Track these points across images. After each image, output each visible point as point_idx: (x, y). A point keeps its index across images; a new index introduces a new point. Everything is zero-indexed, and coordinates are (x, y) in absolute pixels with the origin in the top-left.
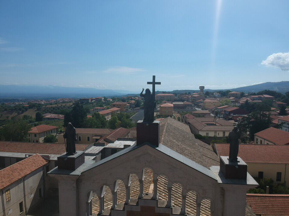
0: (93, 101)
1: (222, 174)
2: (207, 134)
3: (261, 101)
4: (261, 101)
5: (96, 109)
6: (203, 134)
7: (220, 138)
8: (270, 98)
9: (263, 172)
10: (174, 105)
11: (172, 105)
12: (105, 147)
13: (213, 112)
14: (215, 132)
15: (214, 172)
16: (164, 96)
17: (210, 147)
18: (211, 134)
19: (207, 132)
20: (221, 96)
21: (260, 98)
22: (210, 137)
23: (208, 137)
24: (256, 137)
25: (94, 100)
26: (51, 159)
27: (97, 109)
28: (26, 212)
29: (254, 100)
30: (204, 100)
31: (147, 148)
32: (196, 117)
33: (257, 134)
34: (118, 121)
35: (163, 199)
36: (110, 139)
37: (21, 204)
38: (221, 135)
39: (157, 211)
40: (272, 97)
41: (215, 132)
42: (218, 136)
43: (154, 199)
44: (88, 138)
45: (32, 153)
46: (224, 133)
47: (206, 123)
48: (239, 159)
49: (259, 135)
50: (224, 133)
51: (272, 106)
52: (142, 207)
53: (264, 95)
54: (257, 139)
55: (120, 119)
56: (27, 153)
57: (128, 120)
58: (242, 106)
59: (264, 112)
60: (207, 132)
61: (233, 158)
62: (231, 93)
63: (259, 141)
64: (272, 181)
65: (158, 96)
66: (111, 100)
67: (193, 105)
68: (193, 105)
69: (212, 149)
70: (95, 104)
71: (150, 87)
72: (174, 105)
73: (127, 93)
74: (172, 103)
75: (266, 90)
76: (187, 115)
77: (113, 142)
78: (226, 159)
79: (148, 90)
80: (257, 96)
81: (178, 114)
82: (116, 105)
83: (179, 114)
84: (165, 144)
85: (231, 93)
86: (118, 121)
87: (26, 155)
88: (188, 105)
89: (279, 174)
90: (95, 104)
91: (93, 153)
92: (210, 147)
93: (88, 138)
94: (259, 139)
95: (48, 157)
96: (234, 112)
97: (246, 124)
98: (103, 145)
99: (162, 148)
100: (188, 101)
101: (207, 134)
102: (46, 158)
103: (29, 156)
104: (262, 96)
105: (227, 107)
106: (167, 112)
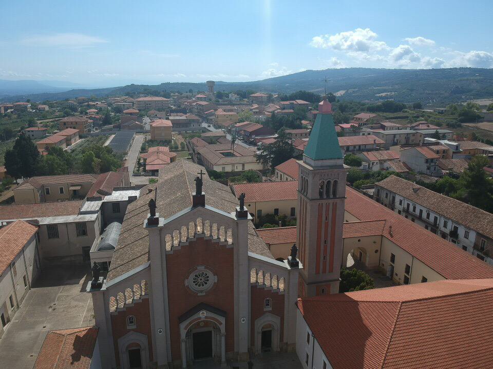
0: (9, 111)
1: (237, 216)
2: (224, 168)
3: (292, 111)
4: (292, 111)
5: (29, 131)
6: (218, 169)
7: (238, 173)
8: (306, 104)
9: (278, 209)
10: (173, 122)
11: (168, 123)
12: (103, 201)
13: (229, 132)
14: (233, 165)
15: (233, 215)
16: (150, 101)
17: (228, 188)
18: (229, 169)
19: (223, 166)
20: (240, 100)
21: (292, 106)
22: (227, 172)
23: (225, 173)
24: (277, 171)
25: (11, 108)
26: (40, 224)
27: (32, 131)
28: (29, 286)
29: (284, 109)
30: (216, 110)
31: (200, 208)
32: (209, 143)
33: (276, 167)
34: (95, 159)
35: (207, 233)
36: (104, 189)
37: (24, 277)
38: (240, 169)
39: (205, 239)
40: (307, 103)
41: (233, 165)
42: (236, 170)
43: (203, 233)
44: (61, 189)
45: (11, 219)
46: (243, 165)
47: (222, 152)
48: (245, 207)
49: (280, 167)
50: (243, 165)
51: (304, 118)
52: (182, 247)
53: (297, 101)
54: (277, 173)
55: (98, 156)
56: (3, 219)
57: (111, 157)
58: (266, 123)
59: (287, 141)
60: (223, 166)
61: (242, 208)
62: (253, 95)
63: (279, 176)
64: (285, 217)
65: (140, 101)
66: (47, 108)
67: (201, 120)
68: (201, 120)
69: (230, 190)
70: (15, 116)
71: (199, 175)
72: (173, 122)
73: (69, 87)
74: (167, 119)
75: (300, 91)
76: (194, 140)
77: (110, 194)
78: (238, 208)
79: (198, 178)
80: (288, 103)
81: (178, 136)
82: (68, 122)
83: (180, 137)
84: (210, 204)
85: (253, 95)
86: (95, 159)
87: (2, 223)
88: (194, 121)
89: (293, 210)
90: (15, 116)
91: (93, 210)
92: (228, 188)
93: (61, 189)
94: (280, 173)
95: (37, 222)
96: (257, 133)
97: (267, 155)
98: (100, 199)
99: (207, 207)
100: (191, 112)
101: (224, 168)
102: (35, 224)
103: (8, 223)
104: (294, 102)
105: (247, 125)
106: (163, 135)
